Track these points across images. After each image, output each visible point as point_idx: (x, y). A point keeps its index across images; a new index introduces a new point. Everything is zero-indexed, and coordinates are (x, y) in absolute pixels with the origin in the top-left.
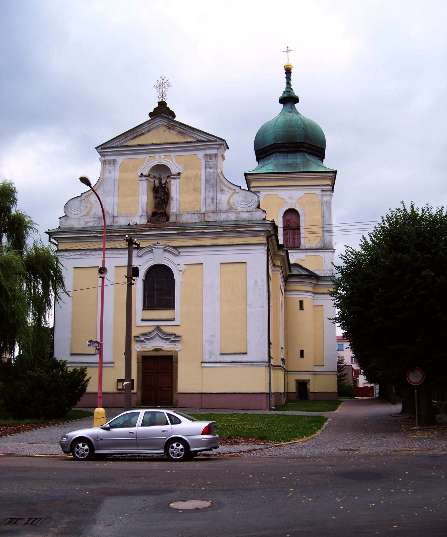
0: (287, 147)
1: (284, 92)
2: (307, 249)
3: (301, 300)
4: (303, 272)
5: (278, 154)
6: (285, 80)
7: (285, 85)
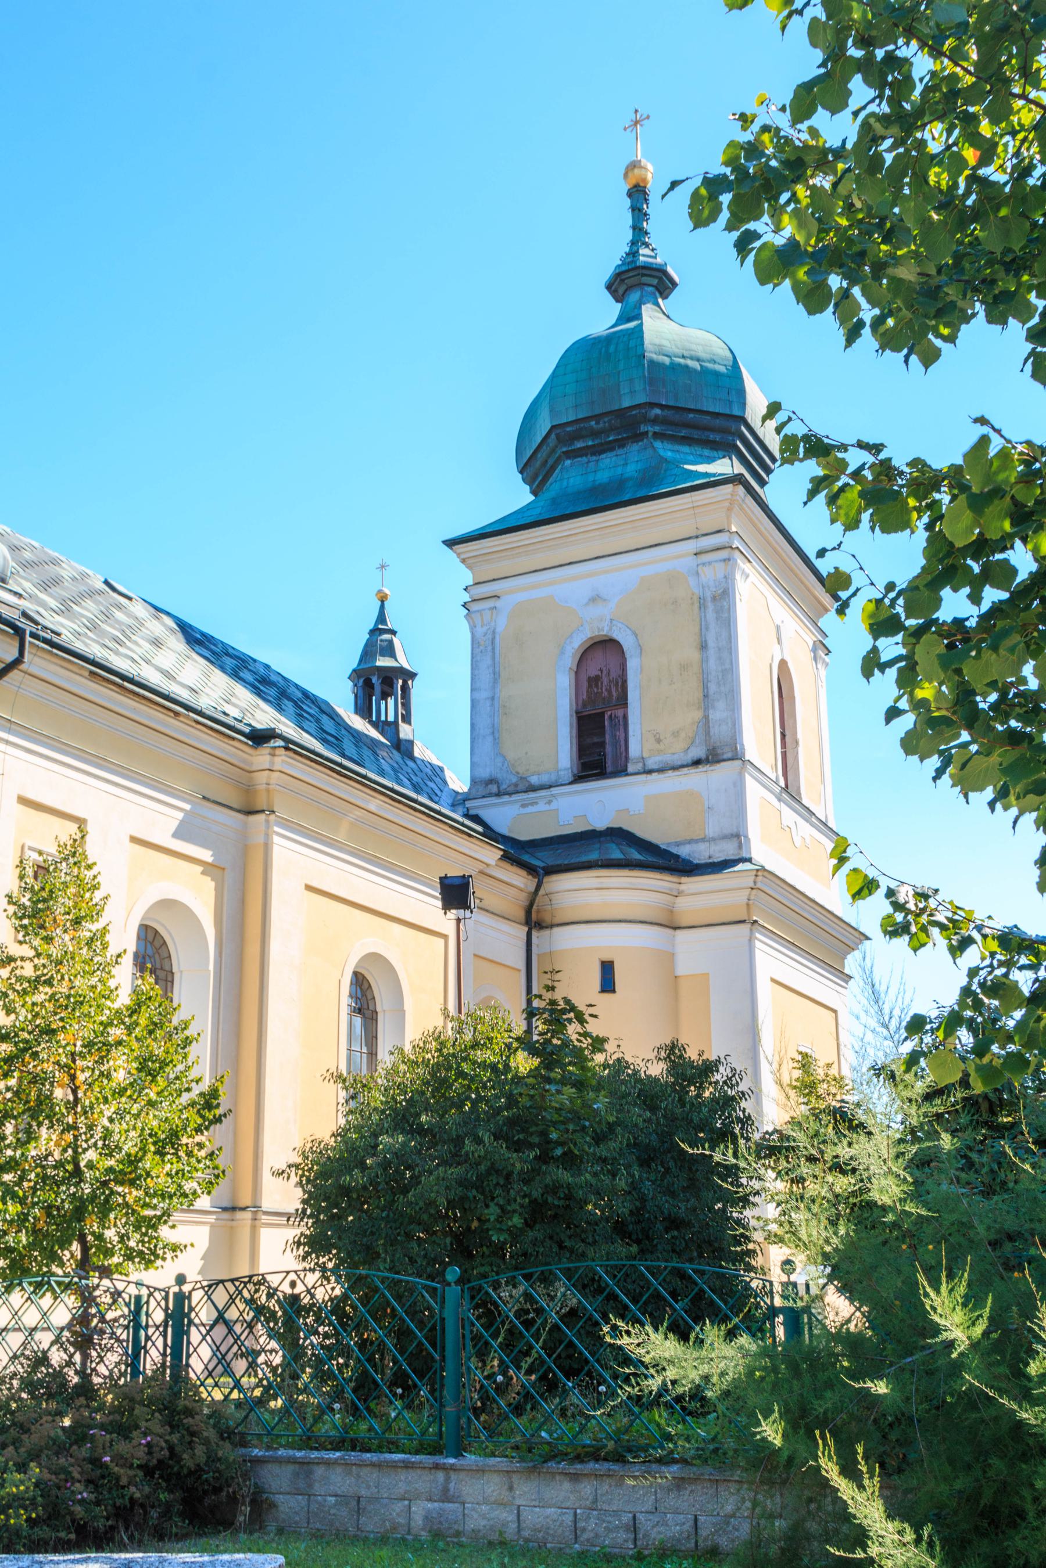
0: (594, 434)
1: (627, 254)
2: (650, 772)
3: (606, 957)
4: (636, 855)
5: (568, 462)
6: (628, 219)
7: (629, 235)
